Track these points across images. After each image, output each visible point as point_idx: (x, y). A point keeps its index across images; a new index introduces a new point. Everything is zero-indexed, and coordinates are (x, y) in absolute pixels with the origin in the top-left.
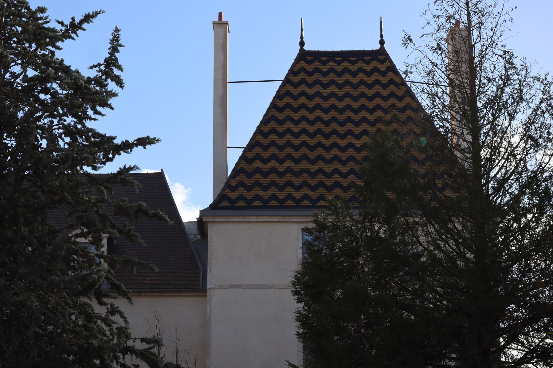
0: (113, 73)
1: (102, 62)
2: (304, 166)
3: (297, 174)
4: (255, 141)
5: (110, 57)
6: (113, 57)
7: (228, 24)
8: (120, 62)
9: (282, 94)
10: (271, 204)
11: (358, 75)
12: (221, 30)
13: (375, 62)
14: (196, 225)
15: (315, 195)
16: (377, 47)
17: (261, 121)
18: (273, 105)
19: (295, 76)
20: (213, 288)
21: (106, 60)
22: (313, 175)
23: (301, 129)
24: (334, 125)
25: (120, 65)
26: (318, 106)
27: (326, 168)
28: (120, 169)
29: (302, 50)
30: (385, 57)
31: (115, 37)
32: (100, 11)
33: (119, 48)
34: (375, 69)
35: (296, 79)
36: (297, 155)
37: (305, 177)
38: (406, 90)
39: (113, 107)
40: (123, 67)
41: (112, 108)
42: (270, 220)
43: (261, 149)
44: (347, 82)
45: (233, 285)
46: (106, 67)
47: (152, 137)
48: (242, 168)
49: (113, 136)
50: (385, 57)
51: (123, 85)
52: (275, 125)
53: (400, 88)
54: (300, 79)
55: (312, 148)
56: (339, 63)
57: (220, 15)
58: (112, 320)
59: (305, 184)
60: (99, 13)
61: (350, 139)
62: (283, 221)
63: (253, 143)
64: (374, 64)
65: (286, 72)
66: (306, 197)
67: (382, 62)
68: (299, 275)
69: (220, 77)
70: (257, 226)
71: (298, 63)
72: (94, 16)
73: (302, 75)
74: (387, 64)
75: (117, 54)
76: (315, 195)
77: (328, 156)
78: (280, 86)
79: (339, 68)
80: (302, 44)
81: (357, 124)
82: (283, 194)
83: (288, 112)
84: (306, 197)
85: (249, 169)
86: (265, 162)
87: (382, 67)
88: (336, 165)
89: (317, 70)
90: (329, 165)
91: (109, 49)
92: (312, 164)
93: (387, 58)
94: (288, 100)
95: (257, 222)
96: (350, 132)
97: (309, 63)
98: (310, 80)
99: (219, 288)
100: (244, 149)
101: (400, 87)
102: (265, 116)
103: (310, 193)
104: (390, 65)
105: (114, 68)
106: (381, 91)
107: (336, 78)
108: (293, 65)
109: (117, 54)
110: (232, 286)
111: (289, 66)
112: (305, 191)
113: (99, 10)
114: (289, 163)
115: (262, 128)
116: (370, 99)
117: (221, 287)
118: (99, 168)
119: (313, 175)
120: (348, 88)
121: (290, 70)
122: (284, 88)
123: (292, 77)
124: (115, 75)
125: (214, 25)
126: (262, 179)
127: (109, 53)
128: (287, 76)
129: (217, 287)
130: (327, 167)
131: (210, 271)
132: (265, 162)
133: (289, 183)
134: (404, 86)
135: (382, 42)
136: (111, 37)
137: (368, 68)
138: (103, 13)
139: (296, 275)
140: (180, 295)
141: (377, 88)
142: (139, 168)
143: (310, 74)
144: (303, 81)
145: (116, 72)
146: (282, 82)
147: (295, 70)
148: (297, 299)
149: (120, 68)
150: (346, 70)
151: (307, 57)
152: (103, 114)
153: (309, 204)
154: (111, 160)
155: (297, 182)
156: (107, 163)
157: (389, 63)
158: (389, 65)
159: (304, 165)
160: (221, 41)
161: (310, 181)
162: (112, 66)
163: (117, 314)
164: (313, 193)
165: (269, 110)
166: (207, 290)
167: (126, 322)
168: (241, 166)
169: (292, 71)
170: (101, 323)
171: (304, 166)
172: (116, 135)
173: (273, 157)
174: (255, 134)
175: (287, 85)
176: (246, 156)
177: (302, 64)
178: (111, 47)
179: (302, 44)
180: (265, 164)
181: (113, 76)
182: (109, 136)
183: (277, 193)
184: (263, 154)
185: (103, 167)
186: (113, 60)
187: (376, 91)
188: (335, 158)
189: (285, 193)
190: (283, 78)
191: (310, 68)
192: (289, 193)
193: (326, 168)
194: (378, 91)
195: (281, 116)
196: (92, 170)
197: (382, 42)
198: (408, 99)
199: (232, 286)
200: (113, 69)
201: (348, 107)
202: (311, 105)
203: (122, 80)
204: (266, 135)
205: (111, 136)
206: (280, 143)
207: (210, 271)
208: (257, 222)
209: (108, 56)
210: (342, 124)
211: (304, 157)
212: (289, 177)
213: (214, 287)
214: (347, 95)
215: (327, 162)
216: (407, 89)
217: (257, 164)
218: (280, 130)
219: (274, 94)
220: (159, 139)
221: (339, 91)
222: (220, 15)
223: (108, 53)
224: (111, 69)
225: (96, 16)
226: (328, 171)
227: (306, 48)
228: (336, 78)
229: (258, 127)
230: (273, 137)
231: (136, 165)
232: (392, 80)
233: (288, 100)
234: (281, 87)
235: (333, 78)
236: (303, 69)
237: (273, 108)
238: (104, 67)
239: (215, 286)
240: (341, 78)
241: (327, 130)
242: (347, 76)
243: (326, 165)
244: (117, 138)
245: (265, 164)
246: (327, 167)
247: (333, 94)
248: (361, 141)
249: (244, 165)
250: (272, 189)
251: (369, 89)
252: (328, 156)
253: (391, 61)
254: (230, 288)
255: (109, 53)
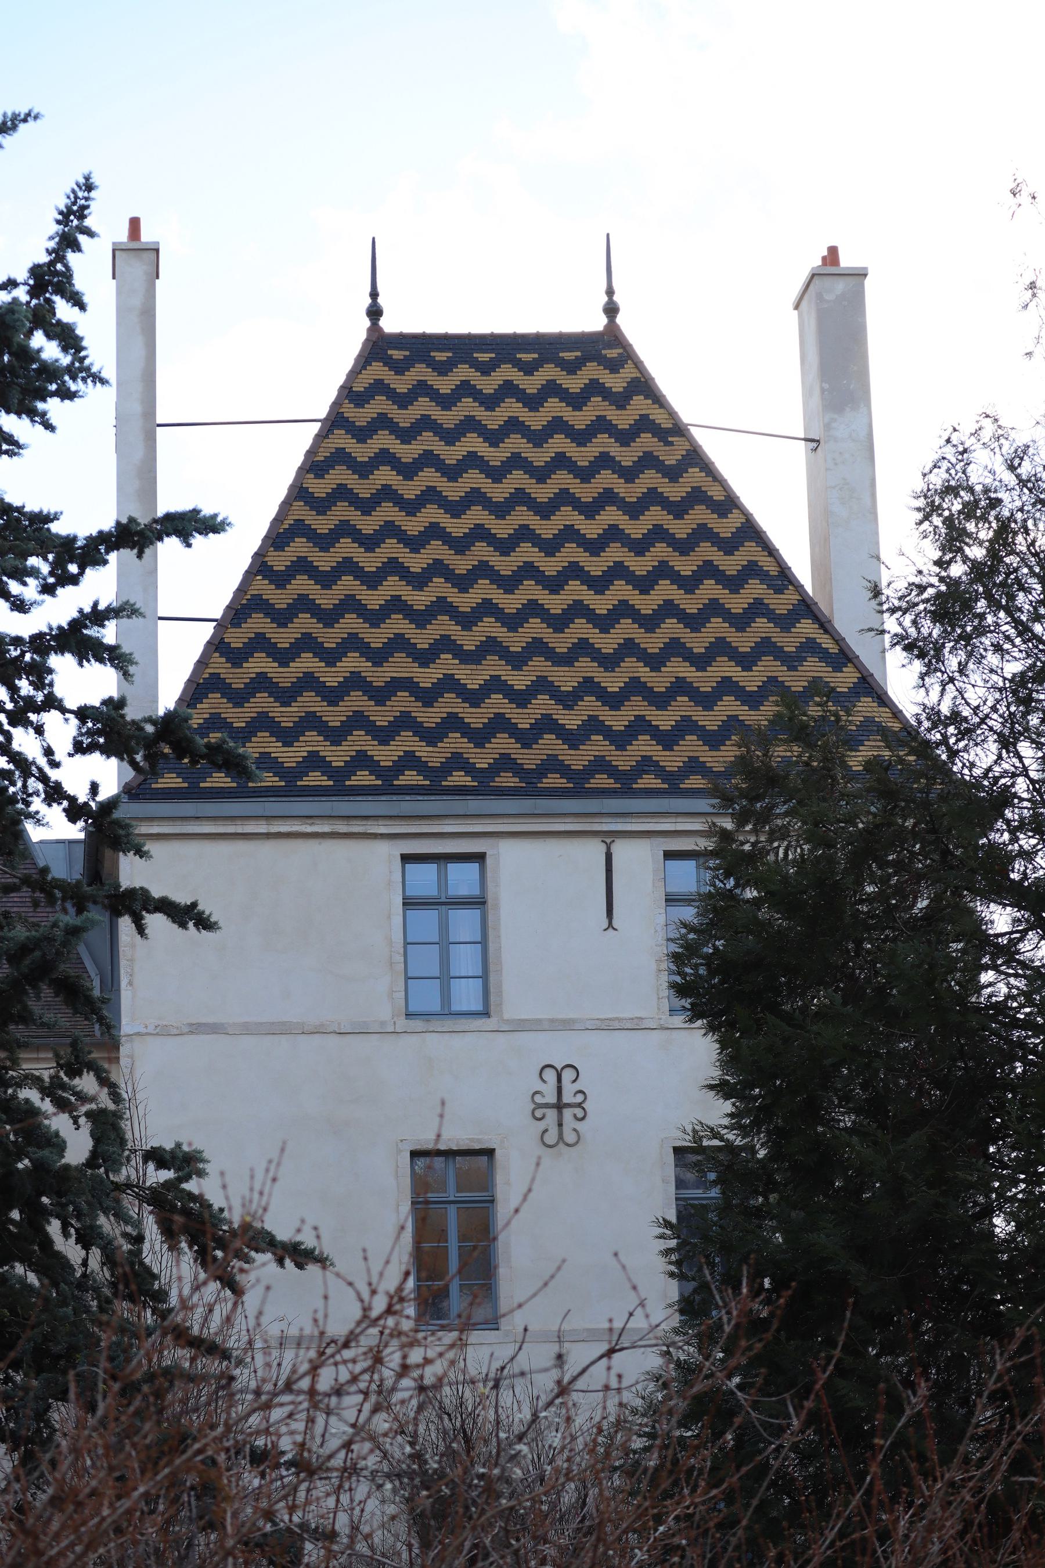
0: (54, 314)
1: (21, 274)
2: (400, 669)
3: (381, 695)
4: (249, 597)
5: (52, 263)
6: (59, 267)
7: (157, 251)
8: (79, 283)
9: (322, 459)
10: (307, 783)
11: (545, 404)
12: (136, 269)
13: (592, 365)
14: (80, 852)
15: (438, 755)
16: (597, 323)
17: (266, 538)
18: (298, 493)
19: (357, 406)
20: (138, 1034)
21: (36, 271)
22: (428, 697)
23: (646, 490)
24: (348, 584)
25: (77, 293)
26: (430, 495)
27: (464, 677)
28: (81, 611)
29: (375, 328)
30: (621, 351)
31: (74, 203)
32: (28, 115)
33: (82, 239)
34: (595, 388)
35: (362, 416)
36: (377, 637)
37: (402, 702)
38: (688, 448)
39: (53, 421)
40: (86, 299)
41: (49, 427)
42: (309, 829)
43: (269, 620)
44: (513, 425)
45: (199, 1025)
46: (33, 292)
47: (207, 511)
48: (215, 676)
49: (49, 513)
50: (621, 351)
51: (83, 354)
52: (306, 549)
53: (671, 444)
54: (375, 415)
55: (421, 618)
56: (486, 369)
57: (135, 224)
58: (78, 1089)
59: (405, 722)
60: (25, 120)
61: (530, 591)
62: (345, 834)
63: (244, 602)
64: (592, 371)
65: (332, 395)
66: (409, 761)
67: (614, 366)
68: (691, 936)
69: (137, 408)
70: (266, 850)
71: (364, 368)
72: (10, 129)
73: (379, 405)
74: (628, 372)
75: (71, 257)
76: (438, 755)
77: (469, 640)
78: (317, 436)
79: (488, 384)
80: (375, 313)
81: (550, 548)
82: (342, 753)
83: (342, 511)
84: (409, 761)
85: (238, 678)
86: (284, 657)
87: (616, 382)
88: (493, 667)
89: (422, 389)
90: (474, 667)
91: (51, 238)
92: (424, 664)
93: (627, 356)
94: (340, 475)
95: (268, 836)
96: (529, 571)
97: (399, 368)
98: (405, 417)
99: (157, 1034)
100: (215, 623)
101: (670, 439)
102: (277, 521)
103: (423, 751)
104: (639, 375)
105: (57, 299)
106: (615, 450)
107: (480, 413)
108: (354, 374)
109: (71, 257)
110: (197, 1029)
111: (340, 379)
112: (406, 742)
113: (24, 111)
114: (353, 663)
115: (266, 559)
116: (585, 475)
117: (163, 1032)
118: (31, 604)
119: (428, 697)
120: (515, 443)
121: (342, 388)
122: (327, 440)
123: (349, 411)
124: (59, 322)
125: (117, 253)
126: (276, 709)
127: (49, 252)
128: (336, 405)
129: (150, 1030)
130: (469, 672)
131: (130, 983)
132: (284, 657)
133: (358, 721)
134: (683, 436)
135: (611, 310)
136: (62, 203)
137: (574, 384)
138: (38, 121)
139: (683, 937)
140: (35, 1056)
141: (603, 443)
142: (142, 610)
143: (403, 401)
144: (383, 422)
145: (64, 311)
146: (319, 424)
147: (358, 388)
148: (689, 1007)
149: (77, 301)
150: (509, 389)
151: (390, 352)
152: (21, 442)
153: (420, 783)
154: (74, 580)
155: (382, 716)
156: (60, 591)
157: (635, 370)
158: (634, 375)
159: (400, 666)
160: (137, 301)
161: (422, 714)
162: (51, 294)
163: (88, 1072)
164: (431, 749)
165: (286, 506)
166: (123, 1040)
167: (116, 1097)
168: (212, 671)
169: (349, 394)
170: (42, 1099)
171: (400, 669)
172: (59, 510)
173: (307, 643)
174: (249, 575)
175: (335, 432)
176: (226, 640)
177: (377, 370)
178: (57, 233)
179: (375, 313)
180: (284, 664)
181: (52, 324)
182: (37, 510)
183: (322, 748)
184: (276, 635)
185: (43, 601)
186: (57, 273)
187: (601, 450)
188: (491, 647)
189: (347, 748)
190: (323, 413)
191: (401, 384)
192: (359, 748)
193: (464, 677)
194: (606, 450)
195: (323, 524)
196: (12, 610)
197: (611, 310)
198: (694, 476)
199: (197, 1029)
200: (54, 302)
201: (520, 497)
202: (410, 490)
203: (82, 339)
204: (279, 580)
205: (41, 512)
206: (326, 601)
207: (130, 983)
208: (268, 836)
209: (44, 258)
210: (373, 581)
211: (399, 643)
212: (356, 701)
213: (144, 1031)
214: (516, 462)
215: (465, 657)
216: (691, 445)
217: (259, 664)
218: (323, 564)
219: (298, 459)
220: (225, 519)
221: (492, 449)
222: (135, 224)
223: (47, 250)
224: (49, 301)
225: (14, 127)
226: (473, 685)
227: (389, 325)
228: (480, 413)
229: (257, 555)
230: (302, 584)
231: (132, 602)
232: (644, 418)
233: (340, 475)
234: (320, 438)
235: (472, 414)
236: (379, 387)
237: (297, 498)
238: (28, 292)
239: (146, 1027)
240: (493, 413)
241: (462, 565)
242: (512, 408)
243: (463, 667)
244: (62, 517)
245: (284, 664)
246: (469, 672)
247: (472, 460)
248: (565, 597)
249: (219, 665)
250: (310, 739)
251: (579, 445)
252: (469, 640)
253: (638, 365)
254: (191, 1033)
255: (49, 252)
